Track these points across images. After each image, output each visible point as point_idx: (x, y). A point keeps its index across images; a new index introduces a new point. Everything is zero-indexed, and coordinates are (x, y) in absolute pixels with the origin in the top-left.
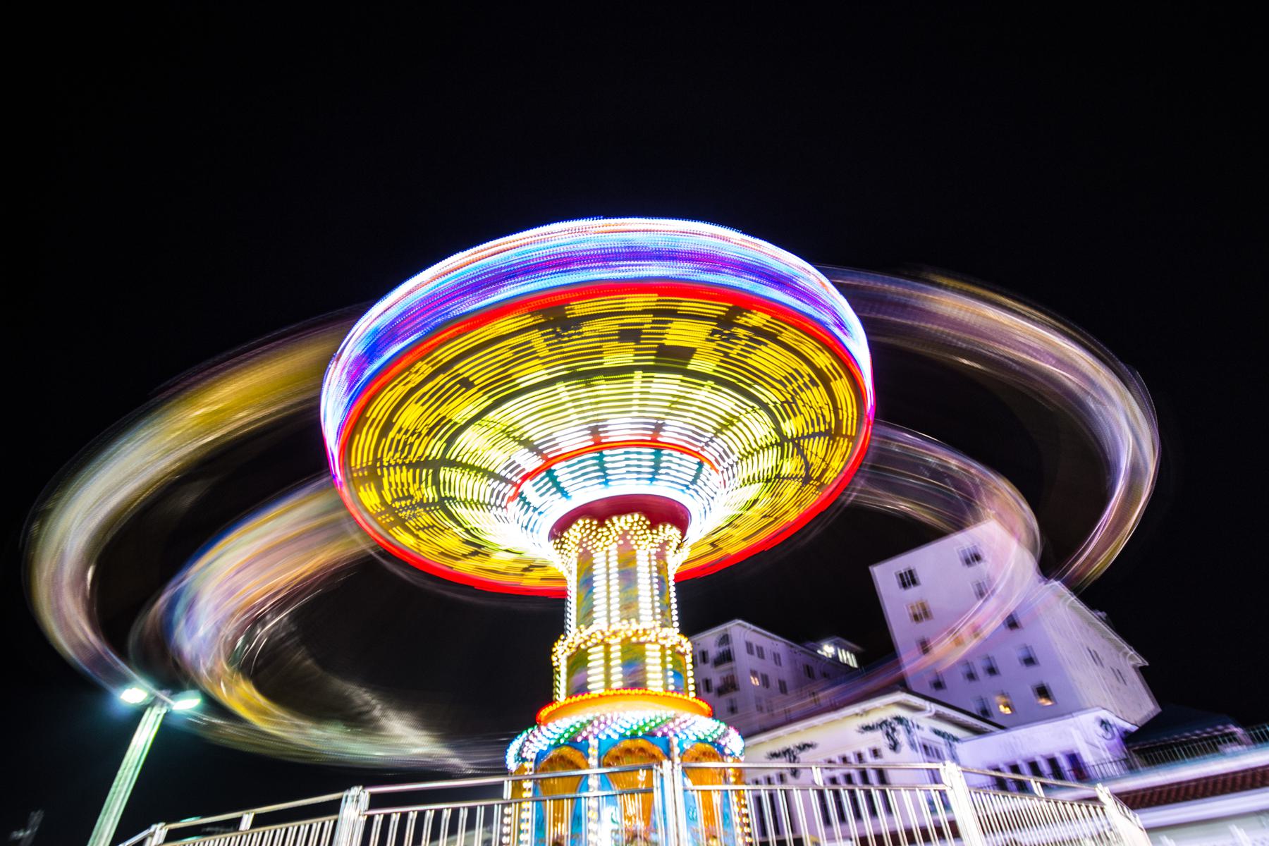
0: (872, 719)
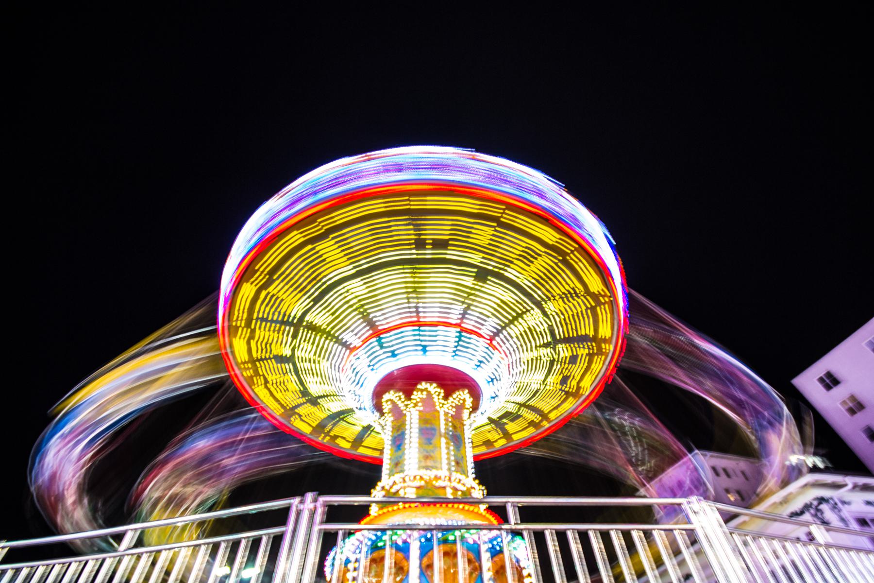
0: (797, 505)
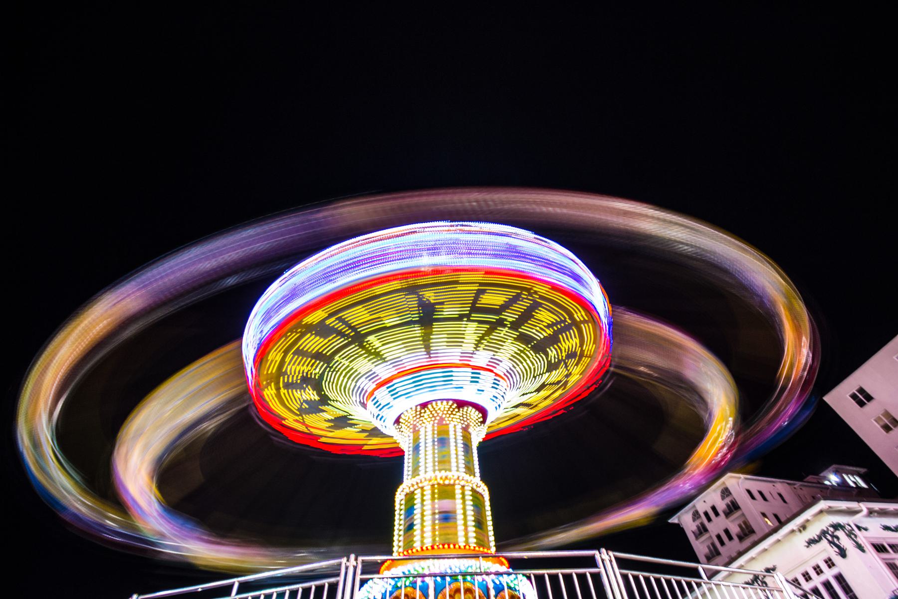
0: (813, 531)
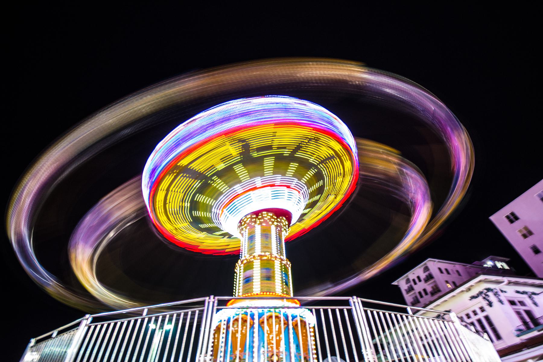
0: (474, 292)
